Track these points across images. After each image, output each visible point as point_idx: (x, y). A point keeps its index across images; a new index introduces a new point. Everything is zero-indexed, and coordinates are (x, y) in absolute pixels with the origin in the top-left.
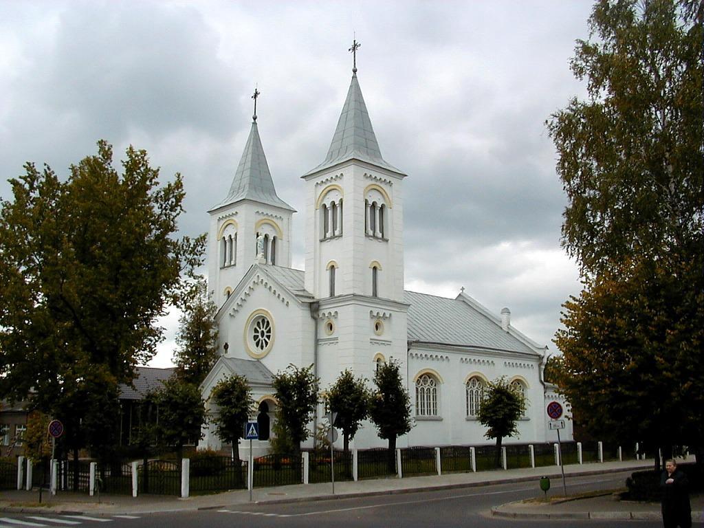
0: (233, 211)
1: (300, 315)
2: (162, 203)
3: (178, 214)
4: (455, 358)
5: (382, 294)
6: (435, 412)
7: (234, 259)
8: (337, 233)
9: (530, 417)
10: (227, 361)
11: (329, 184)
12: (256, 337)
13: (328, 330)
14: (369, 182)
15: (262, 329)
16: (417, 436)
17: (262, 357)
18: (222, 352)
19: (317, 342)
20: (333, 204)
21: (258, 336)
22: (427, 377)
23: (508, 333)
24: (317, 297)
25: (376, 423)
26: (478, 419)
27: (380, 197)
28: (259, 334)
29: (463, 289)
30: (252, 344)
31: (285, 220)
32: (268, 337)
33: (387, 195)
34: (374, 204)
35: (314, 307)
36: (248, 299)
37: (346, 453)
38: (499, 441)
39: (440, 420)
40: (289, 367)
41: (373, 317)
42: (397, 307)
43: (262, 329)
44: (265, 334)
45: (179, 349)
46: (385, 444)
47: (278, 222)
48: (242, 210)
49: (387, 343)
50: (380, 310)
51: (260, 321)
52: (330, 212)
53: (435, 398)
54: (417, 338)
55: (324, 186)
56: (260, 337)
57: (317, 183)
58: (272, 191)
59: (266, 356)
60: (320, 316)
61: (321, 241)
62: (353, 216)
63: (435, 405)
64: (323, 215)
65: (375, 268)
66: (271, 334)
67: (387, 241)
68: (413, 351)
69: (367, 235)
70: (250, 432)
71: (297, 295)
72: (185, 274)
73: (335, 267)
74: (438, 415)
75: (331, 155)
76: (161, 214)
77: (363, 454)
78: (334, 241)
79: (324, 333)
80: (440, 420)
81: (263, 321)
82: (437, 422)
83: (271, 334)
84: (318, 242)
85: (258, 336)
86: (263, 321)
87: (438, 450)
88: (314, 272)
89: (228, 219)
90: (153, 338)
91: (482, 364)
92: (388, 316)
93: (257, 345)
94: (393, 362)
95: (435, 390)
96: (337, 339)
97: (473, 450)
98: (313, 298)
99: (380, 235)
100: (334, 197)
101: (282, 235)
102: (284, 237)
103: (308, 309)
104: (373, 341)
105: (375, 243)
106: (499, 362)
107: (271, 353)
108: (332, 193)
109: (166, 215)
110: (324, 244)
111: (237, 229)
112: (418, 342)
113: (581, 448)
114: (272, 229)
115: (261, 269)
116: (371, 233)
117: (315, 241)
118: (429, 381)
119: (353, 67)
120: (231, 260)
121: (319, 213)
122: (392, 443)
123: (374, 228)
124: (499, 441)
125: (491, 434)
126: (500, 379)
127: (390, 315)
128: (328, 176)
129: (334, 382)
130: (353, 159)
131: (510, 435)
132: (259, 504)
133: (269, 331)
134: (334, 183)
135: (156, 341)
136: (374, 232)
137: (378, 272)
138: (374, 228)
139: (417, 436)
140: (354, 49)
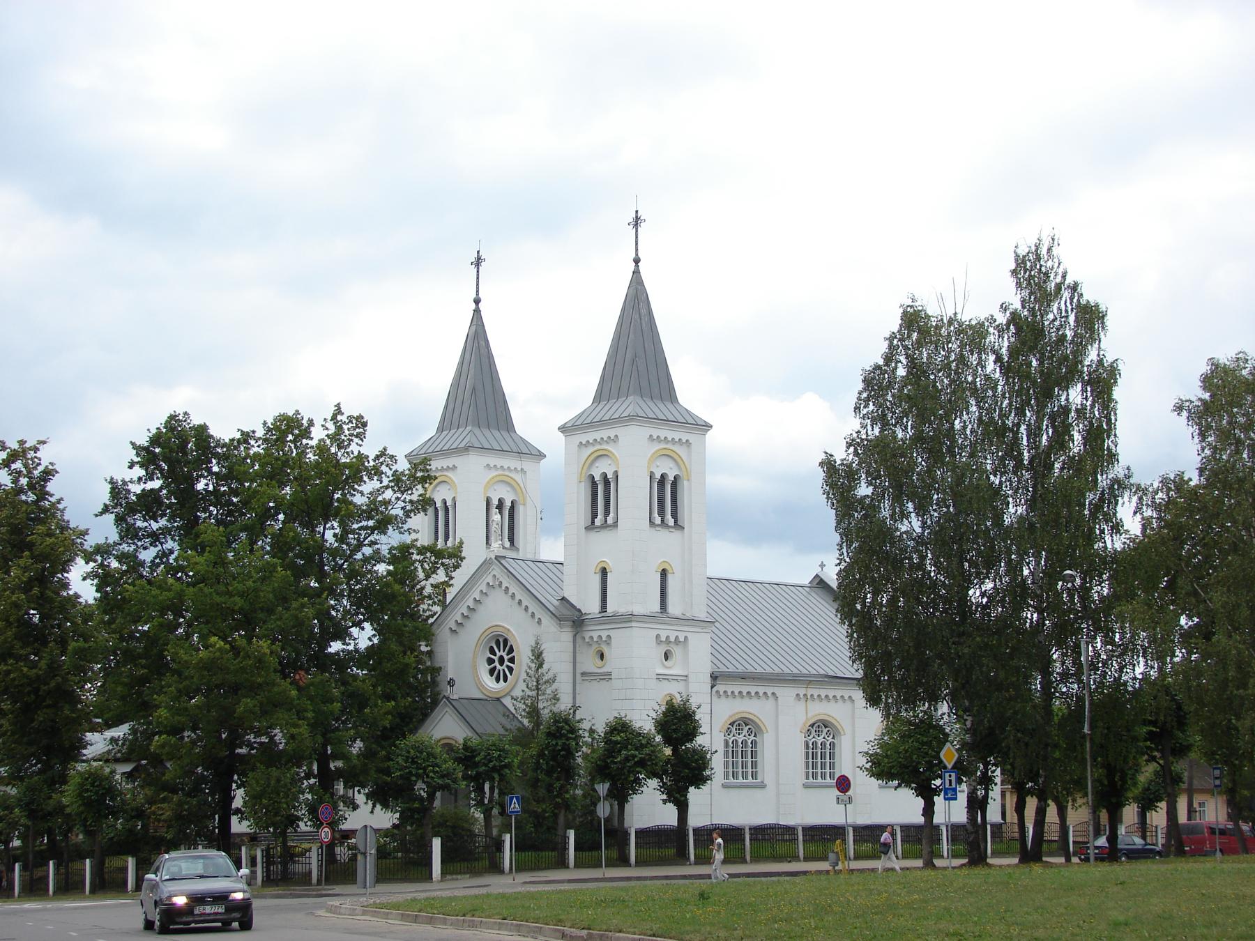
4: (787, 694)
6: (754, 776)
8: (610, 520)
14: (657, 446)
16: (711, 805)
20: (605, 476)
22: (742, 724)
27: (672, 464)
29: (822, 565)
32: (512, 660)
50: (670, 632)
55: (591, 449)
58: (509, 426)
62: (634, 498)
63: (754, 765)
68: (720, 687)
69: (651, 522)
86: (498, 643)
87: (747, 831)
92: (682, 639)
96: (609, 674)
99: (671, 522)
116: (658, 520)
121: (584, 492)
123: (662, 513)
127: (686, 638)
128: (597, 435)
137: (670, 578)
138: (662, 513)
139: (711, 805)
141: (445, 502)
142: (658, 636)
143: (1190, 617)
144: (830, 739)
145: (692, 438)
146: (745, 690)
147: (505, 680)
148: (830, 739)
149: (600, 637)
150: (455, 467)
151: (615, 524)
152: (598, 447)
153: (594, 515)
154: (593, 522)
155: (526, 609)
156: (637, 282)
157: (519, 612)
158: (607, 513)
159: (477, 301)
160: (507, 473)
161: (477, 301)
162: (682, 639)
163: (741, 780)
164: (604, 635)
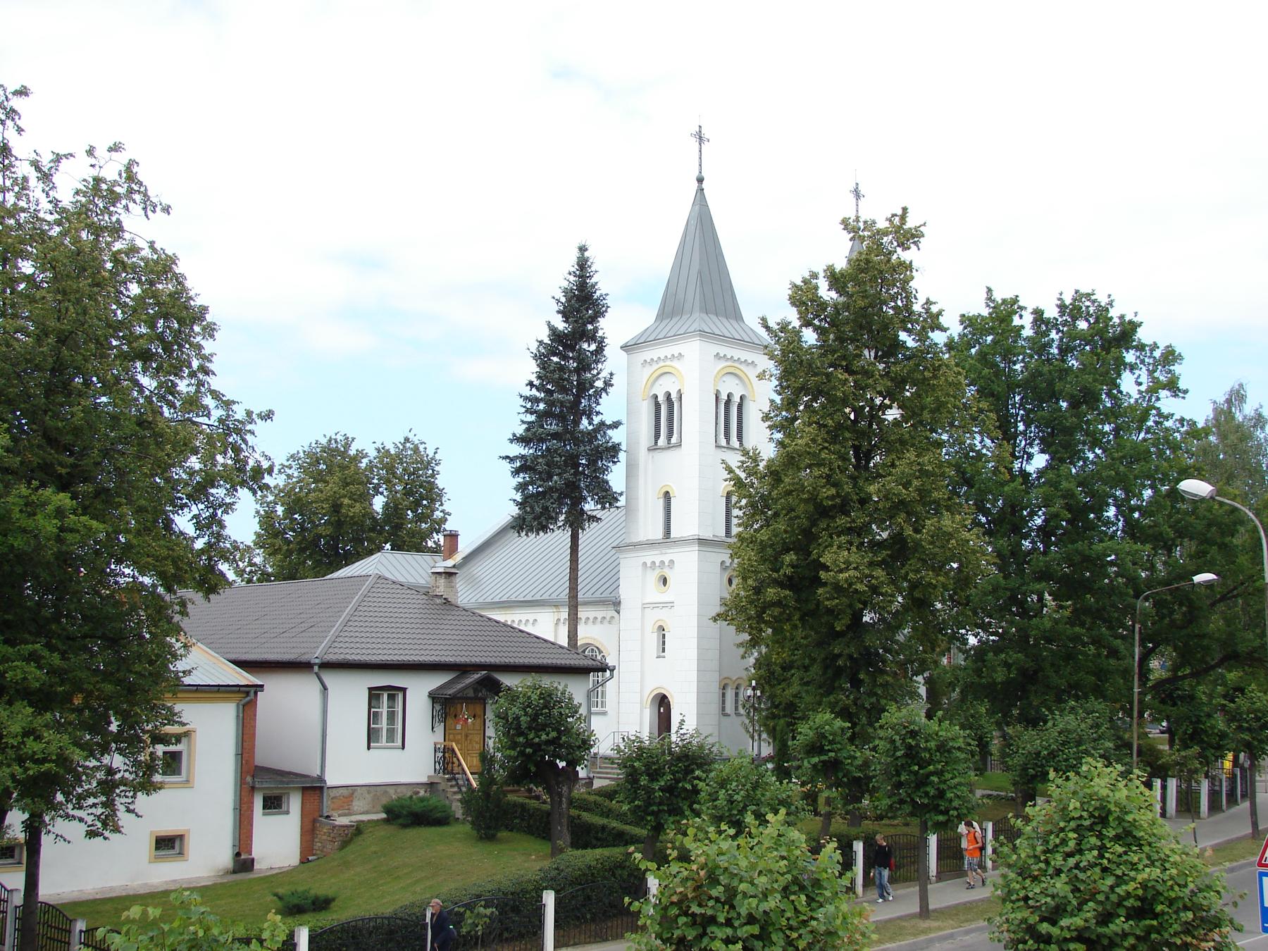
8: (674, 440)
14: (723, 364)
69: (718, 446)
116: (723, 442)
141: (668, 396)
142: (645, 564)
151: (679, 445)
152: (662, 364)
153: (657, 436)
154: (656, 443)
159: (700, 180)
160: (736, 365)
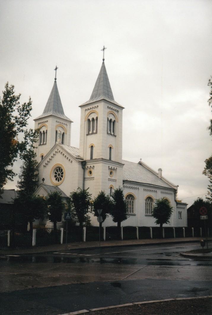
0: (46, 120)
1: (76, 167)
2: (21, 112)
3: (28, 118)
4: (141, 188)
5: (113, 159)
7: (45, 141)
9: (136, 214)
10: (44, 186)
11: (91, 110)
12: (55, 176)
13: (89, 174)
15: (59, 173)
17: (59, 184)
18: (41, 182)
19: (84, 179)
21: (57, 176)
23: (161, 179)
24: (85, 159)
25: (112, 215)
26: (152, 215)
28: (57, 175)
30: (54, 179)
31: (68, 126)
32: (62, 176)
33: (116, 116)
34: (111, 120)
35: (83, 164)
36: (53, 159)
37: (101, 227)
38: (161, 225)
39: (135, 215)
40: (78, 189)
41: (109, 169)
42: (120, 165)
43: (59, 173)
44: (60, 175)
45: (20, 180)
46: (116, 224)
47: (65, 126)
48: (50, 120)
49: (115, 181)
50: (112, 166)
51: (58, 169)
52: (91, 123)
53: (133, 205)
54: (126, 179)
55: (89, 111)
56: (58, 176)
57: (86, 110)
58: (62, 113)
59: (61, 184)
60: (86, 168)
61: (87, 135)
62: (102, 125)
63: (133, 208)
64: (88, 125)
65: (110, 148)
66: (63, 175)
67: (116, 136)
68: (125, 185)
69: (108, 133)
70: (67, 217)
71: (76, 158)
72: (29, 146)
73: (93, 146)
74: (134, 213)
75: (92, 97)
76: (20, 118)
77: (108, 228)
78: (93, 135)
79: (87, 175)
80: (135, 215)
81: (59, 169)
82: (133, 216)
83: (63, 175)
84: (86, 135)
85: (61, 174)
86: (59, 169)
88: (84, 148)
89: (43, 123)
90: (11, 174)
91: (152, 192)
92: (115, 168)
93: (56, 179)
94: (120, 188)
95: (133, 202)
96: (93, 178)
97: (151, 228)
98: (83, 159)
100: (94, 116)
101: (66, 132)
102: (68, 133)
103: (80, 164)
104: (109, 180)
105: (111, 137)
106: (159, 191)
107: (63, 184)
108: (44, 127)
109: (23, 118)
110: (89, 137)
111: (47, 128)
112: (127, 181)
113: (201, 230)
114: (62, 129)
115: (59, 146)
116: (109, 132)
117: (84, 135)
118: (131, 198)
119: (103, 57)
120: (44, 142)
121: (86, 122)
122: (119, 224)
123: (110, 130)
124: (161, 225)
125: (158, 222)
126: (162, 198)
127: (116, 168)
129: (96, 196)
130: (104, 99)
131: (166, 223)
132: (70, 250)
133: (62, 173)
134: (94, 109)
135: (13, 176)
136: (110, 132)
138: (110, 130)
140: (104, 50)
141: (44, 131)
142: (109, 167)
143: (50, 213)
144: (151, 202)
145: (119, 110)
146: (129, 186)
147: (59, 181)
148: (151, 202)
149: (91, 167)
150: (47, 121)
155: (68, 158)
156: (103, 68)
157: (65, 159)
158: (93, 130)
159: (56, 79)
161: (56, 79)
162: (115, 168)
163: (149, 214)
164: (92, 166)
